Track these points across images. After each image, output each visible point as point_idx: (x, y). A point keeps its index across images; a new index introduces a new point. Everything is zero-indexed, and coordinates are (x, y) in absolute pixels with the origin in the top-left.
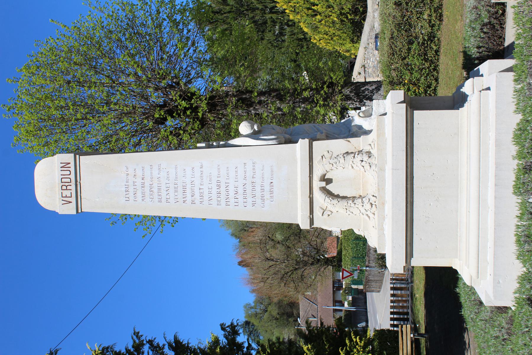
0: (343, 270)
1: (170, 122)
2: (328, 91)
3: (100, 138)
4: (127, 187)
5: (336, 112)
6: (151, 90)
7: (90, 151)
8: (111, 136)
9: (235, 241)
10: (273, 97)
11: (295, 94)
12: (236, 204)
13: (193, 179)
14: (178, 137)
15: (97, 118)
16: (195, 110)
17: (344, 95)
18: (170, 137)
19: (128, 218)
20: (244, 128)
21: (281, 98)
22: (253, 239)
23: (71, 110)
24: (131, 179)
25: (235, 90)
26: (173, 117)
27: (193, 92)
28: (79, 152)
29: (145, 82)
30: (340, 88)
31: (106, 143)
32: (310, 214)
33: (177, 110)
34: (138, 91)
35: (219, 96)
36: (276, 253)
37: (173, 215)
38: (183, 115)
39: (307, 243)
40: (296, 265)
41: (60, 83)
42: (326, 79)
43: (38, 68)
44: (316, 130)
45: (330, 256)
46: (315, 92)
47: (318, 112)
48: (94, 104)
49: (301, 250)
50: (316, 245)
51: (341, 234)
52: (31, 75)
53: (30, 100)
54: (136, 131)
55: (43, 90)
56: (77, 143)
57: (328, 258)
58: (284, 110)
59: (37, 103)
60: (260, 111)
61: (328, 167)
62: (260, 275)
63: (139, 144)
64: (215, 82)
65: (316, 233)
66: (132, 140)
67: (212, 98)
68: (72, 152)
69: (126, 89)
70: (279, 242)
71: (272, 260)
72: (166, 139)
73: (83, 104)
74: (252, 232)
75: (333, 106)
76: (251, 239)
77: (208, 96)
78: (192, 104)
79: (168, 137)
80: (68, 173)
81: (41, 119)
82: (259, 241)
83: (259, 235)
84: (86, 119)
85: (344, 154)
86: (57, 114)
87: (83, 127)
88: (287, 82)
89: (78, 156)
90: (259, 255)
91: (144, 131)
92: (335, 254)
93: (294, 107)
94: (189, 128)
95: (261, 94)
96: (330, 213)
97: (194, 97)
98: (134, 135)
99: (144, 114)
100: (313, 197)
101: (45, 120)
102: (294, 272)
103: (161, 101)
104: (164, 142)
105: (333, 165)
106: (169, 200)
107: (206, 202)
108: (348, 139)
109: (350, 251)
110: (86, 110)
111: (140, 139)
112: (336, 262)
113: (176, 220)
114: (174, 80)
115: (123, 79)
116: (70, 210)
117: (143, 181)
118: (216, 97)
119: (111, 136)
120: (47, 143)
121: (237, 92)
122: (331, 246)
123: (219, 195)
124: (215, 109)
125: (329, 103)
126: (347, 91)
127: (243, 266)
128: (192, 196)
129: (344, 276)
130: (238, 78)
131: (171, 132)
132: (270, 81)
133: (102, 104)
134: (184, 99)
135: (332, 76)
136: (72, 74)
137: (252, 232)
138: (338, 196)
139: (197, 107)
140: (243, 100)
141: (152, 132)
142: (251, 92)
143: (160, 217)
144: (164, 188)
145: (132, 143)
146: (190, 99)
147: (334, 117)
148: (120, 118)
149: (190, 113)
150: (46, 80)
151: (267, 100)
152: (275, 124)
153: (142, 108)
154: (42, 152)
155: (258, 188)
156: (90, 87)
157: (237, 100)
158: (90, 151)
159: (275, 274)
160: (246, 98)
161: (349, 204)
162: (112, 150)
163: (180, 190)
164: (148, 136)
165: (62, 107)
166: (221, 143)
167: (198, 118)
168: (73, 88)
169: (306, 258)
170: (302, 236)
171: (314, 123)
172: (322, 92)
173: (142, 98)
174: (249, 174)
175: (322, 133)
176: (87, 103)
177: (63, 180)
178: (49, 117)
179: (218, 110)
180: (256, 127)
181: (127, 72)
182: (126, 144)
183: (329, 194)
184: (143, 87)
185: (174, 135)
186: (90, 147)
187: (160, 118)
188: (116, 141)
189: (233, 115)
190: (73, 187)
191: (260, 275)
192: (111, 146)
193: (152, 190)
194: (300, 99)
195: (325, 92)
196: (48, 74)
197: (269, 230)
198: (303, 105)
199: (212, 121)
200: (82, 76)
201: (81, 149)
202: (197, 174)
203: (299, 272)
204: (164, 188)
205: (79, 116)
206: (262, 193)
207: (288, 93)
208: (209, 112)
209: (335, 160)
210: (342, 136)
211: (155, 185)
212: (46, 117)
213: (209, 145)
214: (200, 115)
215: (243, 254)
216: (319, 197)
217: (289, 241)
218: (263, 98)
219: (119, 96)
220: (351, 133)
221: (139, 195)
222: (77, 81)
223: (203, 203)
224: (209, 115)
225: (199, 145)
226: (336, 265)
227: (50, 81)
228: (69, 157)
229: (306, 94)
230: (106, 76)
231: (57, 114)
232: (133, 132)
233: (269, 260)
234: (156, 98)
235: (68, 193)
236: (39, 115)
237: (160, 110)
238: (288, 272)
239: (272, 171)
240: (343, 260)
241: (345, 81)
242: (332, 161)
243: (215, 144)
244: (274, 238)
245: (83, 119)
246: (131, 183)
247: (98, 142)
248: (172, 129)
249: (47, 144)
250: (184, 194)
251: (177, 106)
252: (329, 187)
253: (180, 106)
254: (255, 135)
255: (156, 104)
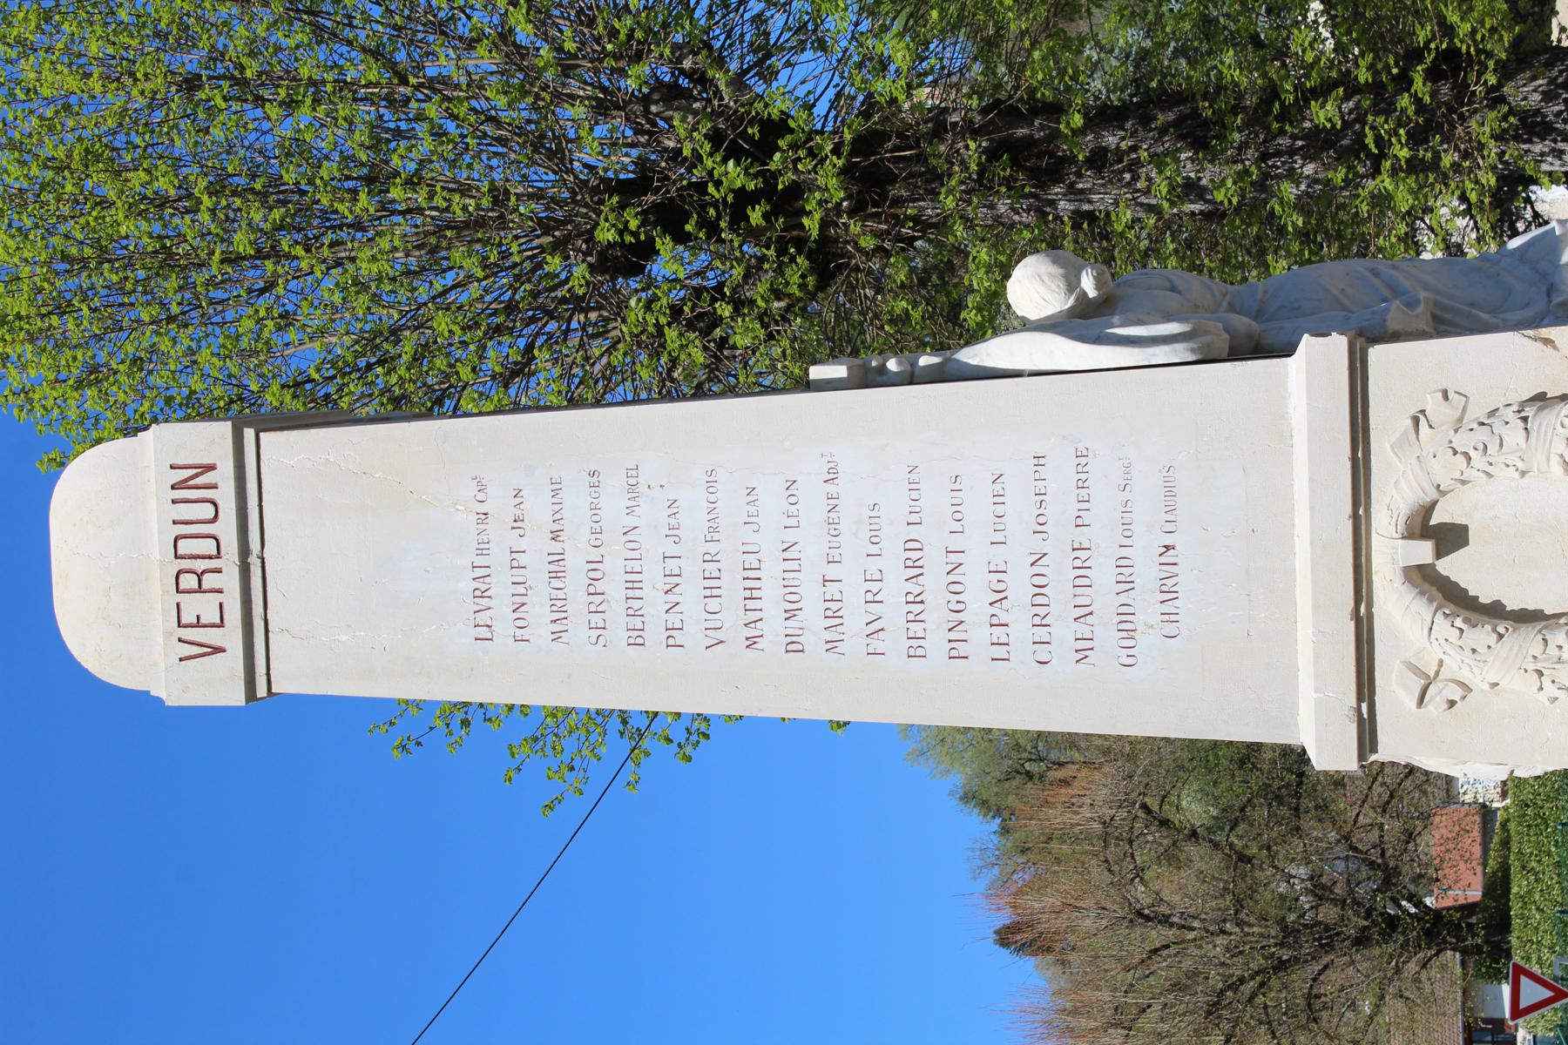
0: (1519, 971)
1: (669, 262)
2: (1433, 95)
3: (341, 344)
4: (481, 573)
5: (1473, 197)
6: (579, 111)
7: (298, 405)
8: (395, 333)
9: (981, 828)
10: (1163, 131)
11: (1269, 111)
12: (1000, 652)
13: (790, 536)
14: (706, 333)
15: (326, 252)
16: (787, 202)
17: (1511, 112)
18: (671, 334)
19: (477, 719)
20: (1034, 287)
21: (1199, 135)
22: (1069, 818)
23: (205, 217)
24: (501, 537)
25: (975, 103)
26: (681, 238)
27: (776, 115)
28: (249, 413)
29: (549, 75)
30: (1493, 80)
31: (369, 367)
32: (1360, 699)
33: (703, 207)
34: (521, 113)
35: (900, 135)
36: (1185, 885)
37: (688, 707)
38: (733, 226)
39: (1333, 836)
40: (1281, 945)
41: (149, 86)
42: (1422, 35)
43: (48, 20)
44: (1385, 292)
45: (1447, 903)
46: (1366, 104)
47: (1382, 201)
48: (311, 182)
49: (1303, 871)
50: (1380, 845)
51: (1504, 795)
52: (13, 54)
53: (14, 169)
54: (511, 308)
55: (71, 123)
56: (235, 370)
57: (1437, 914)
58: (1219, 196)
59: (43, 187)
60: (1101, 201)
61: (1445, 469)
62: (1105, 995)
63: (520, 370)
64: (883, 64)
65: (1377, 789)
66: (491, 353)
67: (866, 143)
68: (209, 415)
69: (462, 111)
70: (1194, 834)
71: (1165, 920)
72: (655, 342)
73: (258, 186)
74: (1065, 783)
75: (1456, 167)
76: (1057, 817)
77: (848, 136)
78: (774, 176)
79: (661, 334)
80: (207, 511)
81: (65, 257)
82: (1096, 826)
83: (1096, 797)
84: (276, 254)
85: (1523, 404)
86: (136, 231)
87: (262, 291)
88: (1229, 56)
89: (249, 433)
90: (1100, 894)
91: (554, 306)
92: (1475, 894)
93: (1266, 176)
94: (762, 288)
95: (1103, 116)
96: (1456, 694)
97: (781, 143)
98: (498, 330)
99: (545, 226)
100: (1370, 615)
101: (84, 262)
102: (1274, 982)
103: (623, 163)
104: (644, 357)
105: (1469, 459)
106: (679, 637)
107: (854, 644)
108: (1544, 332)
109: (1550, 877)
110: (277, 214)
111: (530, 347)
112: (1483, 934)
113: (698, 730)
114: (687, 64)
115: (444, 63)
116: (216, 685)
117: (556, 547)
118: (883, 136)
119: (395, 333)
120: (94, 369)
121: (984, 111)
122: (1454, 855)
123: (916, 608)
124: (884, 196)
125: (1437, 157)
126: (1527, 93)
127: (1022, 948)
128: (790, 615)
129: (1523, 1005)
130: (988, 47)
131: (676, 311)
132: (1144, 55)
133: (350, 184)
134: (735, 153)
135: (1453, 18)
136: (204, 44)
137: (1065, 783)
138: (1495, 611)
139: (797, 190)
140: (1017, 151)
141: (586, 311)
142: (1055, 110)
143: (624, 717)
144: (653, 577)
145: (492, 362)
146: (765, 148)
147: (1461, 222)
148: (434, 250)
149: (765, 216)
150: (88, 76)
151: (1134, 149)
152: (1172, 262)
153: (537, 196)
154: (73, 414)
155: (1103, 575)
156: (290, 104)
157: (986, 151)
158: (298, 405)
159: (1177, 987)
160: (1029, 142)
161: (1552, 651)
162: (396, 401)
163: (732, 585)
164: (568, 330)
165: (162, 202)
166: (925, 361)
167: (800, 243)
168: (212, 111)
169: (1329, 913)
170: (1306, 803)
171: (1362, 254)
172: (1404, 101)
173: (536, 151)
174: (1061, 509)
175: (1411, 304)
176: (276, 181)
177: (185, 547)
178: (103, 250)
179: (898, 202)
180: (1088, 284)
181: (463, 28)
182: (465, 373)
183: (1454, 598)
184: (537, 97)
185: (691, 326)
186: (296, 385)
187: (622, 244)
188: (417, 359)
189: (969, 223)
190: (230, 580)
191: (1105, 995)
192: (394, 379)
193: (599, 586)
194: (1294, 137)
195: (1418, 101)
196: (94, 48)
197: (1146, 773)
198: (1309, 169)
199: (869, 255)
200: (252, 54)
201: (254, 401)
202: (812, 508)
203: (1299, 980)
204: (653, 577)
205: (241, 242)
206: (1123, 599)
207: (1235, 110)
208: (852, 213)
209: (1482, 435)
210: (1514, 316)
211: (614, 569)
212: (88, 251)
213: (865, 368)
214: (812, 224)
215: (1020, 893)
216: (1402, 616)
217: (1243, 826)
218: (1111, 140)
219: (427, 145)
220: (1557, 300)
221: (539, 612)
222: (232, 78)
223: (841, 647)
224: (855, 228)
225: (816, 372)
226: (1478, 949)
227: (105, 78)
228: (209, 440)
229: (1325, 113)
230: (364, 50)
231: (136, 231)
232: (495, 313)
233: (1148, 918)
234: (601, 148)
235: (205, 607)
236: (55, 240)
237: (622, 207)
238: (1242, 980)
239: (1170, 491)
240: (1516, 922)
241: (1517, 43)
242: (1462, 441)
243: (892, 365)
244: (1169, 812)
245: (260, 255)
246: (498, 556)
247: (334, 364)
248: (677, 295)
249: (93, 375)
250: (751, 604)
251: (701, 187)
252: (1452, 567)
253: (718, 184)
254: (1084, 320)
255: (603, 180)
